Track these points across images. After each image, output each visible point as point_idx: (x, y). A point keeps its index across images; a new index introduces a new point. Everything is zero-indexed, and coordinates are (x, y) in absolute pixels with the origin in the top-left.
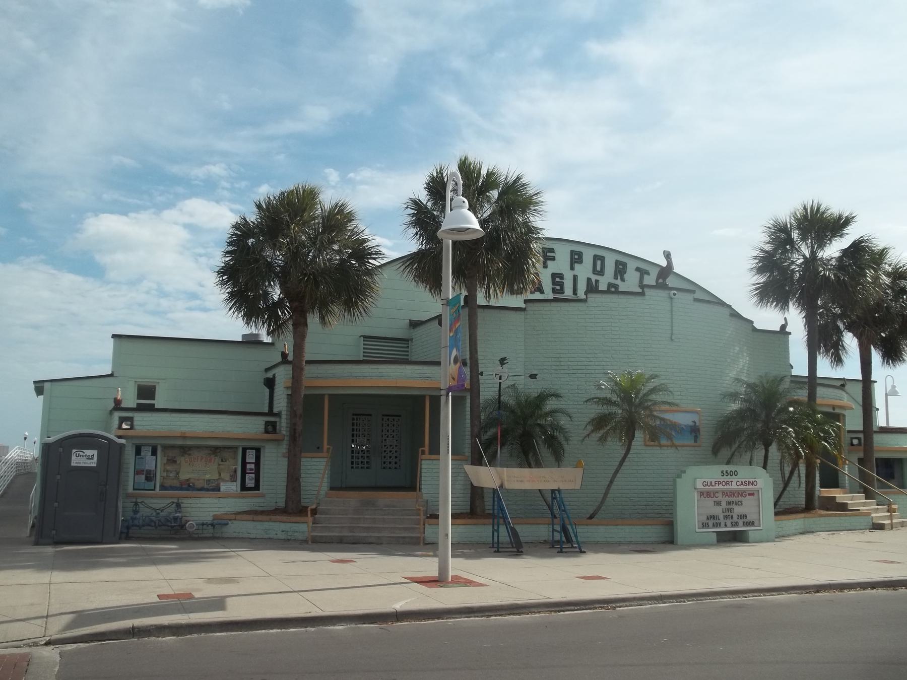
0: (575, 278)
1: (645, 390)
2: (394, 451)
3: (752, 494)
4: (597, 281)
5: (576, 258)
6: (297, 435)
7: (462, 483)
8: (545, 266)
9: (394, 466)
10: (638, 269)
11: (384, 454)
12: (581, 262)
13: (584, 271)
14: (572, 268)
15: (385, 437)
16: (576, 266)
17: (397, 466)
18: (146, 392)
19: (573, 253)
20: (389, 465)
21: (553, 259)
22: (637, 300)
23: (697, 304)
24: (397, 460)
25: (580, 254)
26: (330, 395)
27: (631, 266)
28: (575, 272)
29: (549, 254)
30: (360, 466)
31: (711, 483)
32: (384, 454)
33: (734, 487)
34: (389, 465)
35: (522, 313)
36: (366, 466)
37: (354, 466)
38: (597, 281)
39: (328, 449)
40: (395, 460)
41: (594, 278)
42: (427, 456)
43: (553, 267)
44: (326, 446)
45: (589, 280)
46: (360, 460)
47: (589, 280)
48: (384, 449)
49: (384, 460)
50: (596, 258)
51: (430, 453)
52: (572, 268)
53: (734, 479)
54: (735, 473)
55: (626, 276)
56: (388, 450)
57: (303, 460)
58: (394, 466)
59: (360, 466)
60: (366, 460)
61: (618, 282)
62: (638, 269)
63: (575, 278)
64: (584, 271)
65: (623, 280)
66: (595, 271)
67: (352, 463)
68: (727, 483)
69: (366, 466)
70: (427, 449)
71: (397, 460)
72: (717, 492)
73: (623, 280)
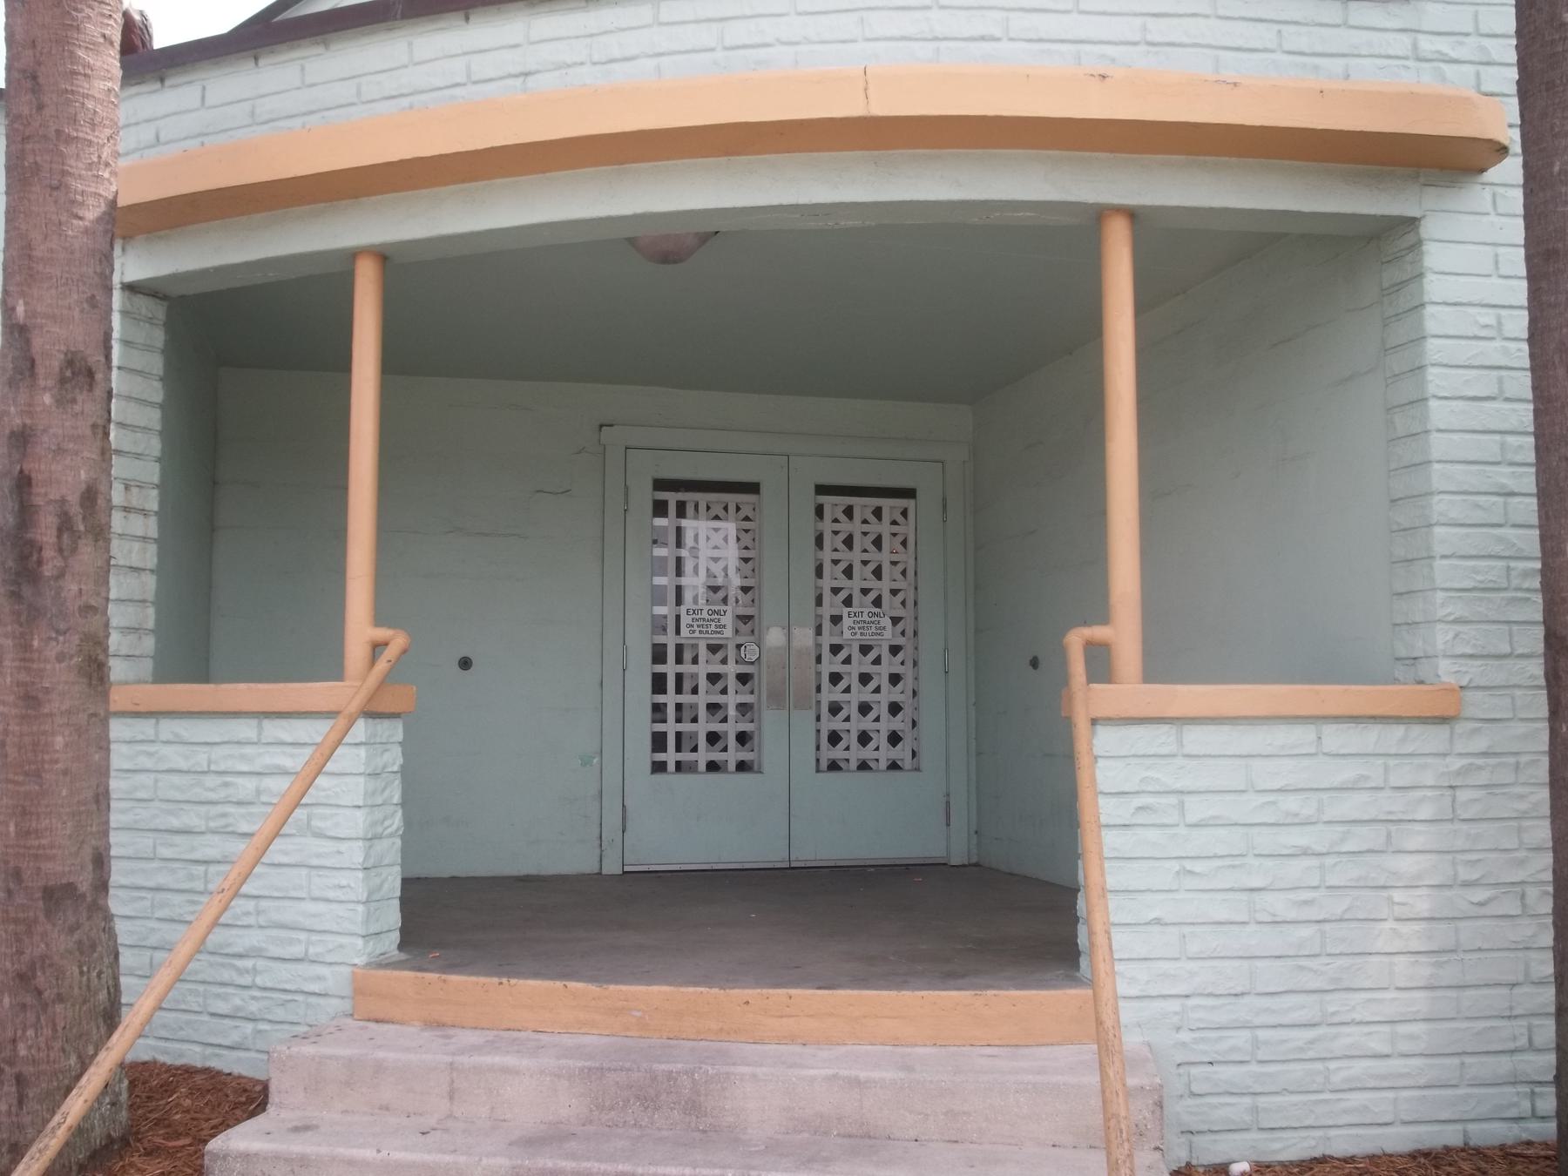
2: (882, 673)
6: (46, 530)
7: (1422, 903)
9: (886, 753)
11: (830, 694)
15: (831, 605)
17: (901, 753)
20: (857, 753)
24: (899, 723)
26: (384, 256)
30: (704, 755)
32: (830, 694)
34: (857, 753)
36: (733, 755)
37: (670, 756)
39: (377, 647)
40: (888, 724)
42: (1128, 690)
44: (359, 626)
46: (703, 727)
48: (830, 665)
49: (830, 724)
51: (1157, 669)
56: (852, 672)
57: (118, 729)
58: (886, 753)
59: (704, 755)
60: (731, 729)
67: (659, 742)
69: (733, 755)
70: (1124, 632)
71: (899, 723)
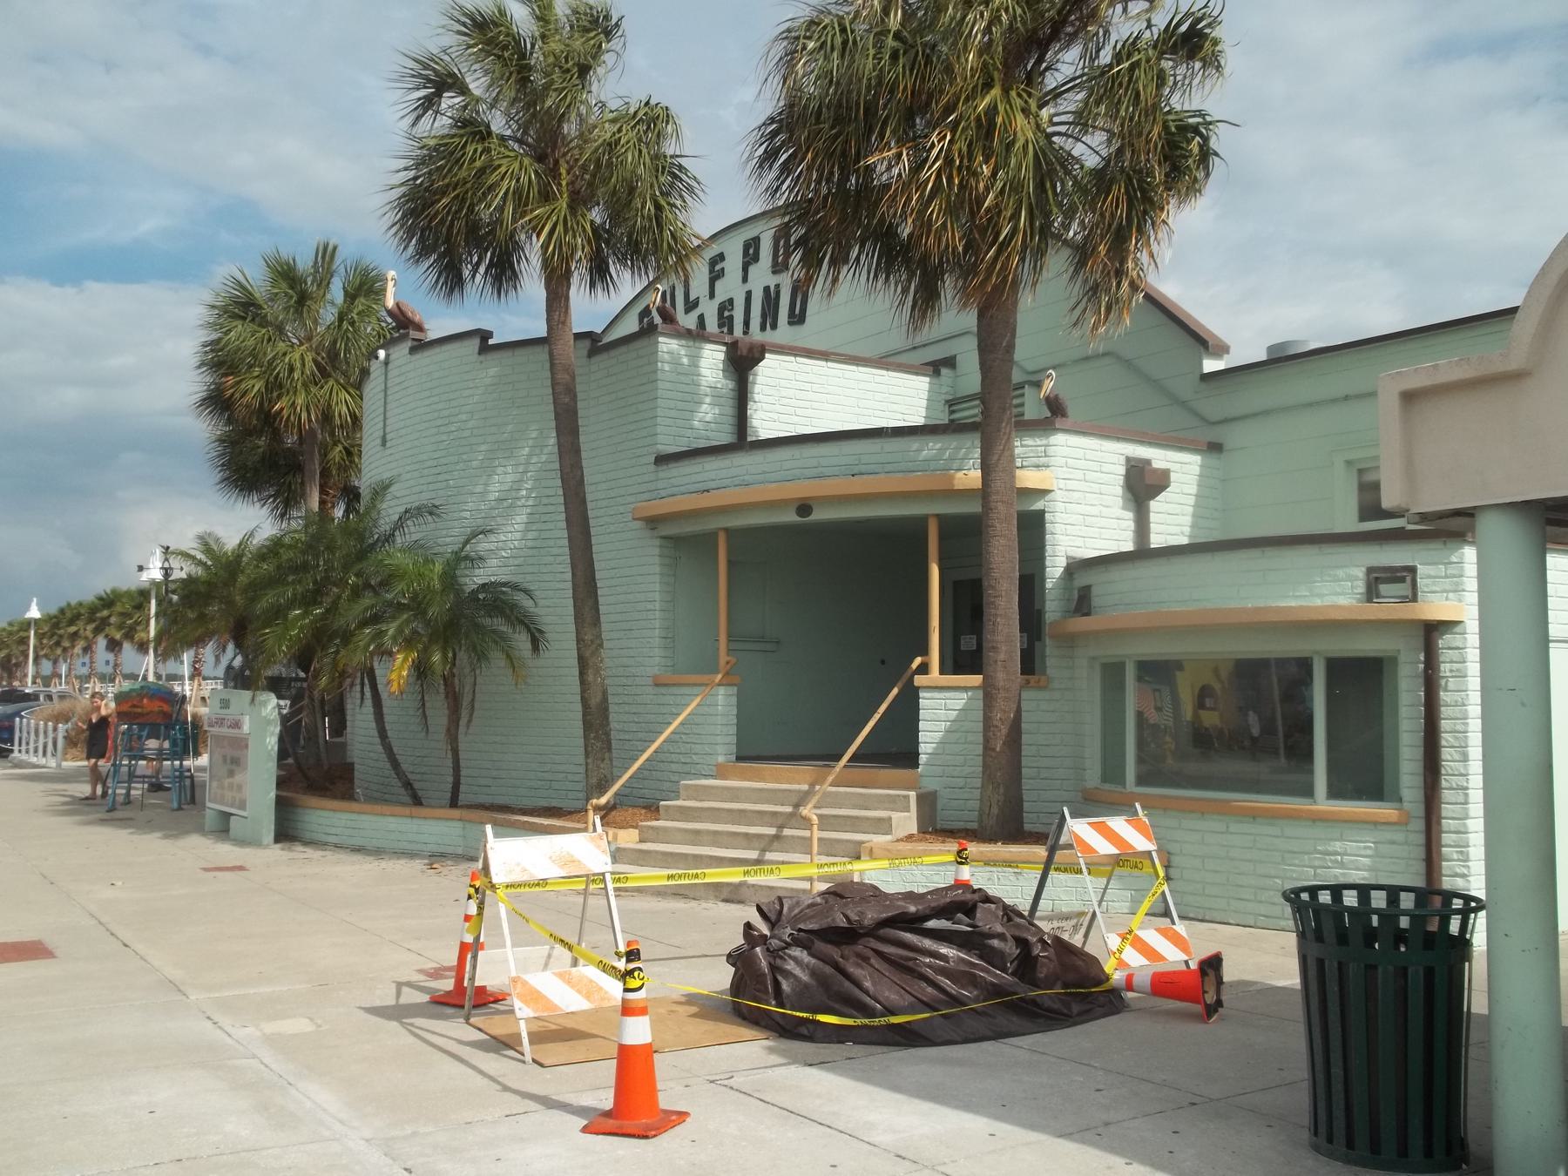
0: (749, 294)
14: (745, 279)
52: (745, 279)
63: (749, 294)
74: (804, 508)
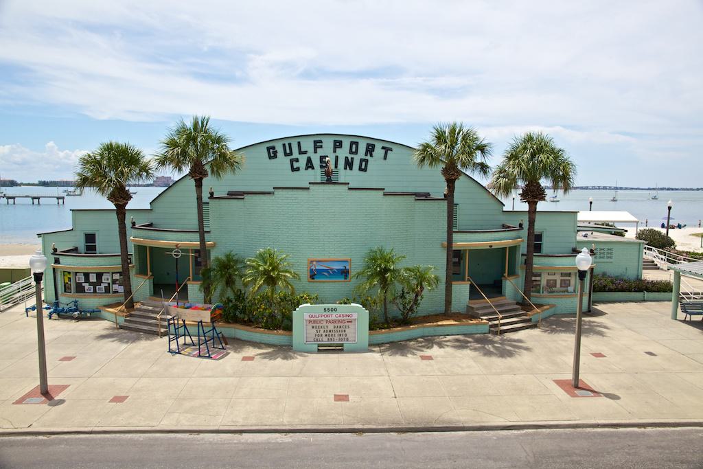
0: (337, 158)
1: (122, 307)
3: (351, 322)
4: (352, 158)
5: (338, 145)
8: (316, 152)
10: (383, 148)
12: (341, 147)
13: (343, 153)
14: (335, 152)
16: (338, 150)
18: (90, 238)
19: (335, 142)
21: (321, 147)
22: (304, 193)
23: (352, 191)
25: (341, 142)
27: (378, 146)
28: (337, 154)
29: (318, 144)
31: (315, 316)
33: (334, 318)
35: (242, 200)
38: (352, 158)
41: (350, 156)
43: (320, 152)
45: (347, 158)
47: (347, 158)
50: (352, 143)
52: (335, 152)
53: (334, 314)
54: (336, 310)
55: (374, 153)
61: (368, 157)
62: (383, 148)
63: (337, 158)
64: (343, 153)
65: (371, 156)
66: (351, 152)
68: (328, 316)
72: (322, 320)
73: (371, 156)
74: (491, 246)
